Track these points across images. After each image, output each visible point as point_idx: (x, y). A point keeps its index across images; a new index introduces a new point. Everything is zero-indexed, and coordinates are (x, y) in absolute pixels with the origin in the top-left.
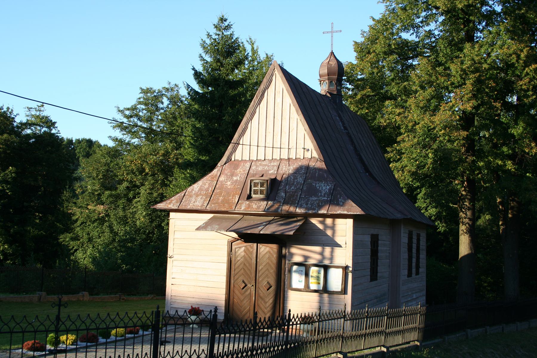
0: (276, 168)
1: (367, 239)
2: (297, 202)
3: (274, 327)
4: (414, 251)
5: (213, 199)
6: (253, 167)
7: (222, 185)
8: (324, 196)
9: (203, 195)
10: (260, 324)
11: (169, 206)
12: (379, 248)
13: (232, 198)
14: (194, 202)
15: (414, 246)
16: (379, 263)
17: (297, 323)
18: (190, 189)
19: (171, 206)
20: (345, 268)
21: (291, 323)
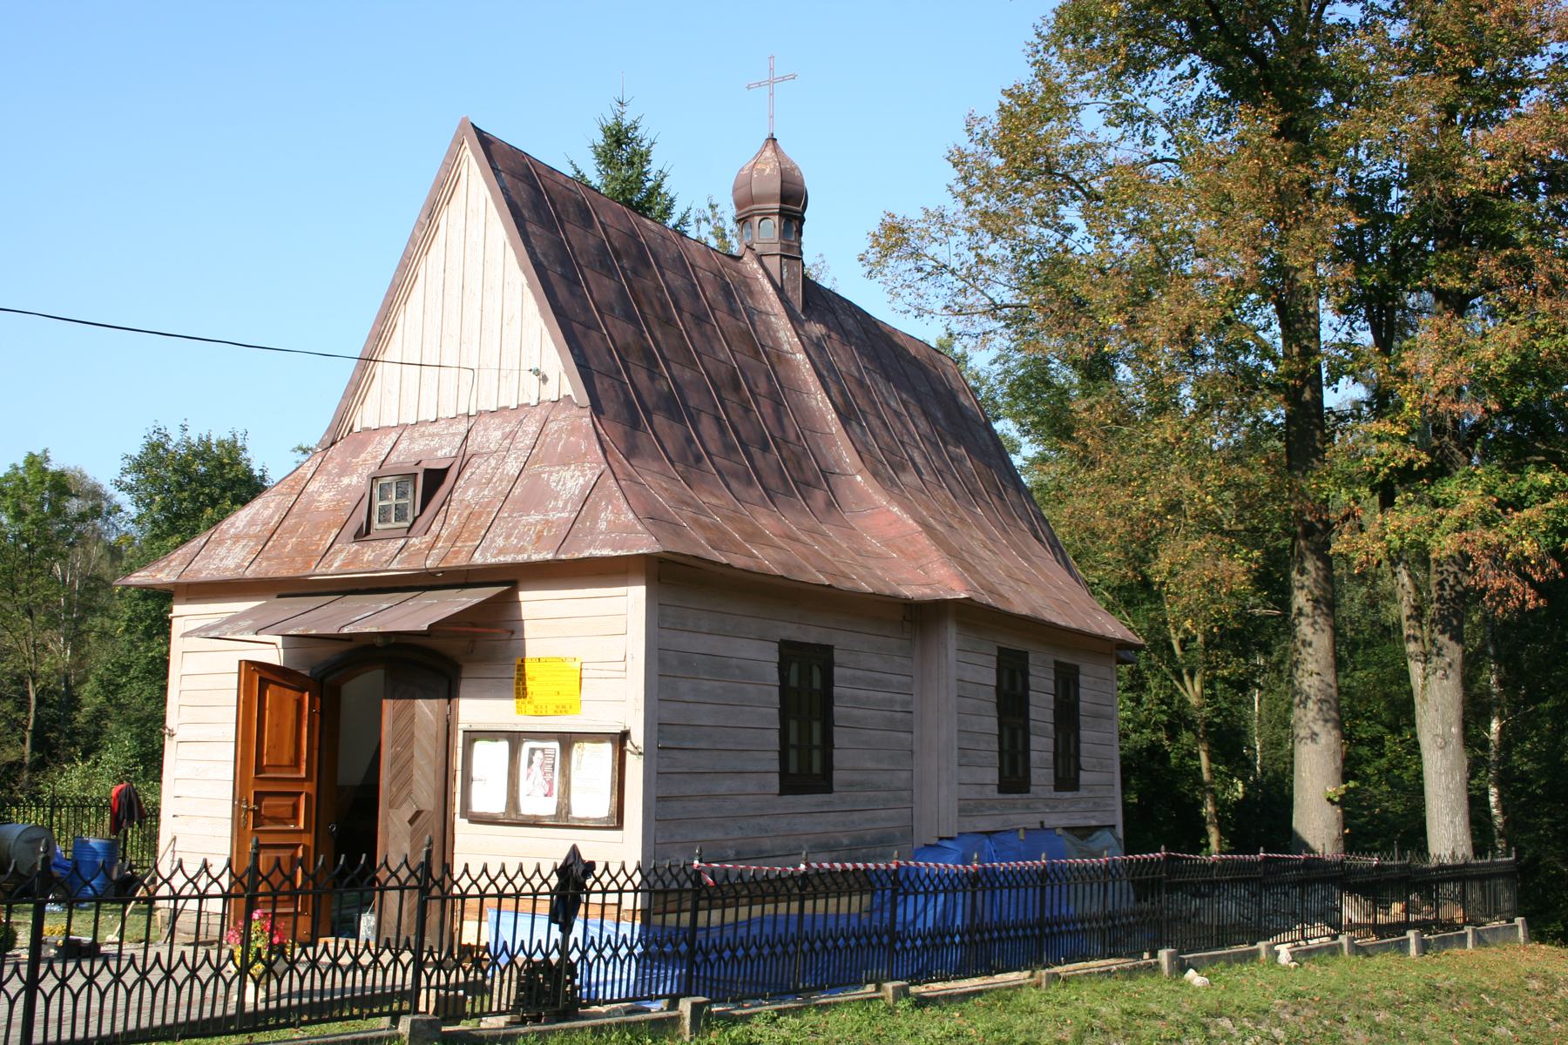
0: (459, 440)
5: (273, 546)
6: (401, 447)
11: (159, 576)
12: (836, 690)
13: (321, 539)
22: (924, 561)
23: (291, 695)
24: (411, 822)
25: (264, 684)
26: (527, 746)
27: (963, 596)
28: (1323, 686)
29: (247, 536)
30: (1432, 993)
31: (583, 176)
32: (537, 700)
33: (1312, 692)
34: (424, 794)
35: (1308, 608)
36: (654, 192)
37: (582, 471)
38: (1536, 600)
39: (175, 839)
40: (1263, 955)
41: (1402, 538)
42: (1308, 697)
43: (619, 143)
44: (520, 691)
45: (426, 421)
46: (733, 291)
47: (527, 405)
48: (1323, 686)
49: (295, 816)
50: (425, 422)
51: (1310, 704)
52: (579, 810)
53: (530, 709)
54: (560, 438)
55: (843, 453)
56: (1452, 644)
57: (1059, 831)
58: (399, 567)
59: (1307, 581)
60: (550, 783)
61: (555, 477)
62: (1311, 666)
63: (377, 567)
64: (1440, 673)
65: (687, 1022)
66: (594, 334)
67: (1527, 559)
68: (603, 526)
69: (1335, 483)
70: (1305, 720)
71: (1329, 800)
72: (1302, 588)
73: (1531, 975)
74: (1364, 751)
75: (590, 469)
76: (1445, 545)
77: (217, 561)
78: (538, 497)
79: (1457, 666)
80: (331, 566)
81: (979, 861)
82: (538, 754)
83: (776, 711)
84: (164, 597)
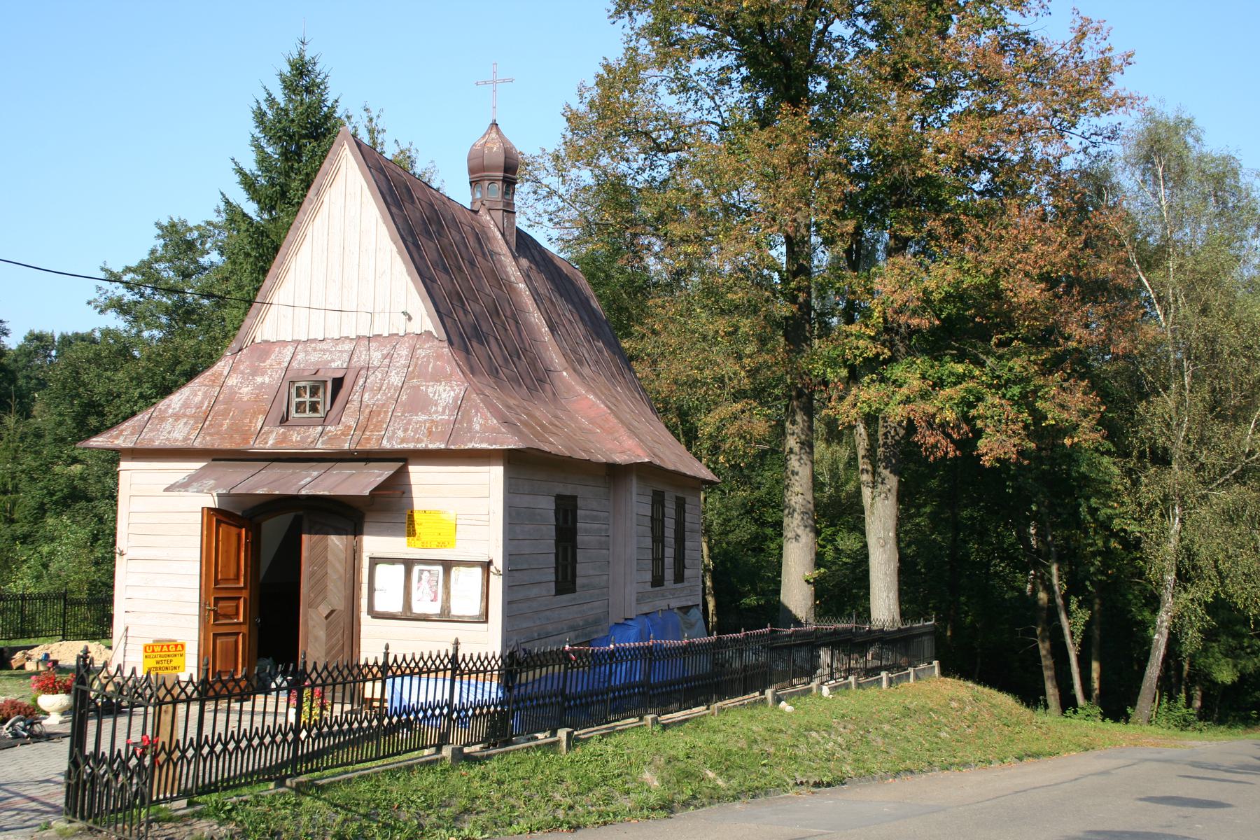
0: (346, 357)
1: (546, 505)
2: (385, 426)
3: (210, 699)
4: (670, 533)
5: (210, 425)
6: (300, 356)
7: (233, 393)
8: (444, 413)
9: (189, 417)
10: (314, 676)
11: (116, 442)
12: (578, 525)
13: (251, 422)
14: (169, 433)
15: (670, 524)
16: (579, 558)
17: (492, 668)
18: (162, 405)
19: (120, 443)
20: (486, 566)
21: (390, 673)
22: (617, 435)
23: (234, 530)
24: (327, 618)
25: (219, 522)
26: (416, 569)
27: (646, 460)
28: (804, 503)
29: (184, 415)
30: (907, 712)
31: (274, 99)
32: (424, 538)
33: (797, 506)
34: (336, 598)
35: (796, 449)
36: (327, 117)
37: (452, 387)
38: (954, 451)
39: (127, 630)
40: (815, 691)
41: (870, 407)
42: (794, 510)
43: (301, 74)
44: (411, 532)
45: (316, 340)
46: (481, 237)
47: (397, 335)
48: (804, 503)
49: (237, 614)
50: (315, 340)
51: (796, 515)
52: (456, 610)
53: (419, 544)
54: (429, 363)
55: (554, 356)
56: (891, 476)
57: (676, 610)
58: (324, 447)
59: (797, 429)
60: (436, 593)
61: (430, 389)
62: (797, 489)
63: (305, 446)
64: (883, 496)
65: (564, 744)
66: (435, 285)
67: (948, 423)
68: (477, 427)
69: (824, 364)
70: (792, 526)
71: (808, 581)
72: (793, 434)
73: (952, 699)
74: (769, 531)
75: (458, 385)
76: (897, 413)
77: (165, 433)
78: (419, 403)
79: (894, 491)
80: (266, 443)
81: (688, 638)
82: (426, 574)
83: (553, 541)
84: (115, 456)
